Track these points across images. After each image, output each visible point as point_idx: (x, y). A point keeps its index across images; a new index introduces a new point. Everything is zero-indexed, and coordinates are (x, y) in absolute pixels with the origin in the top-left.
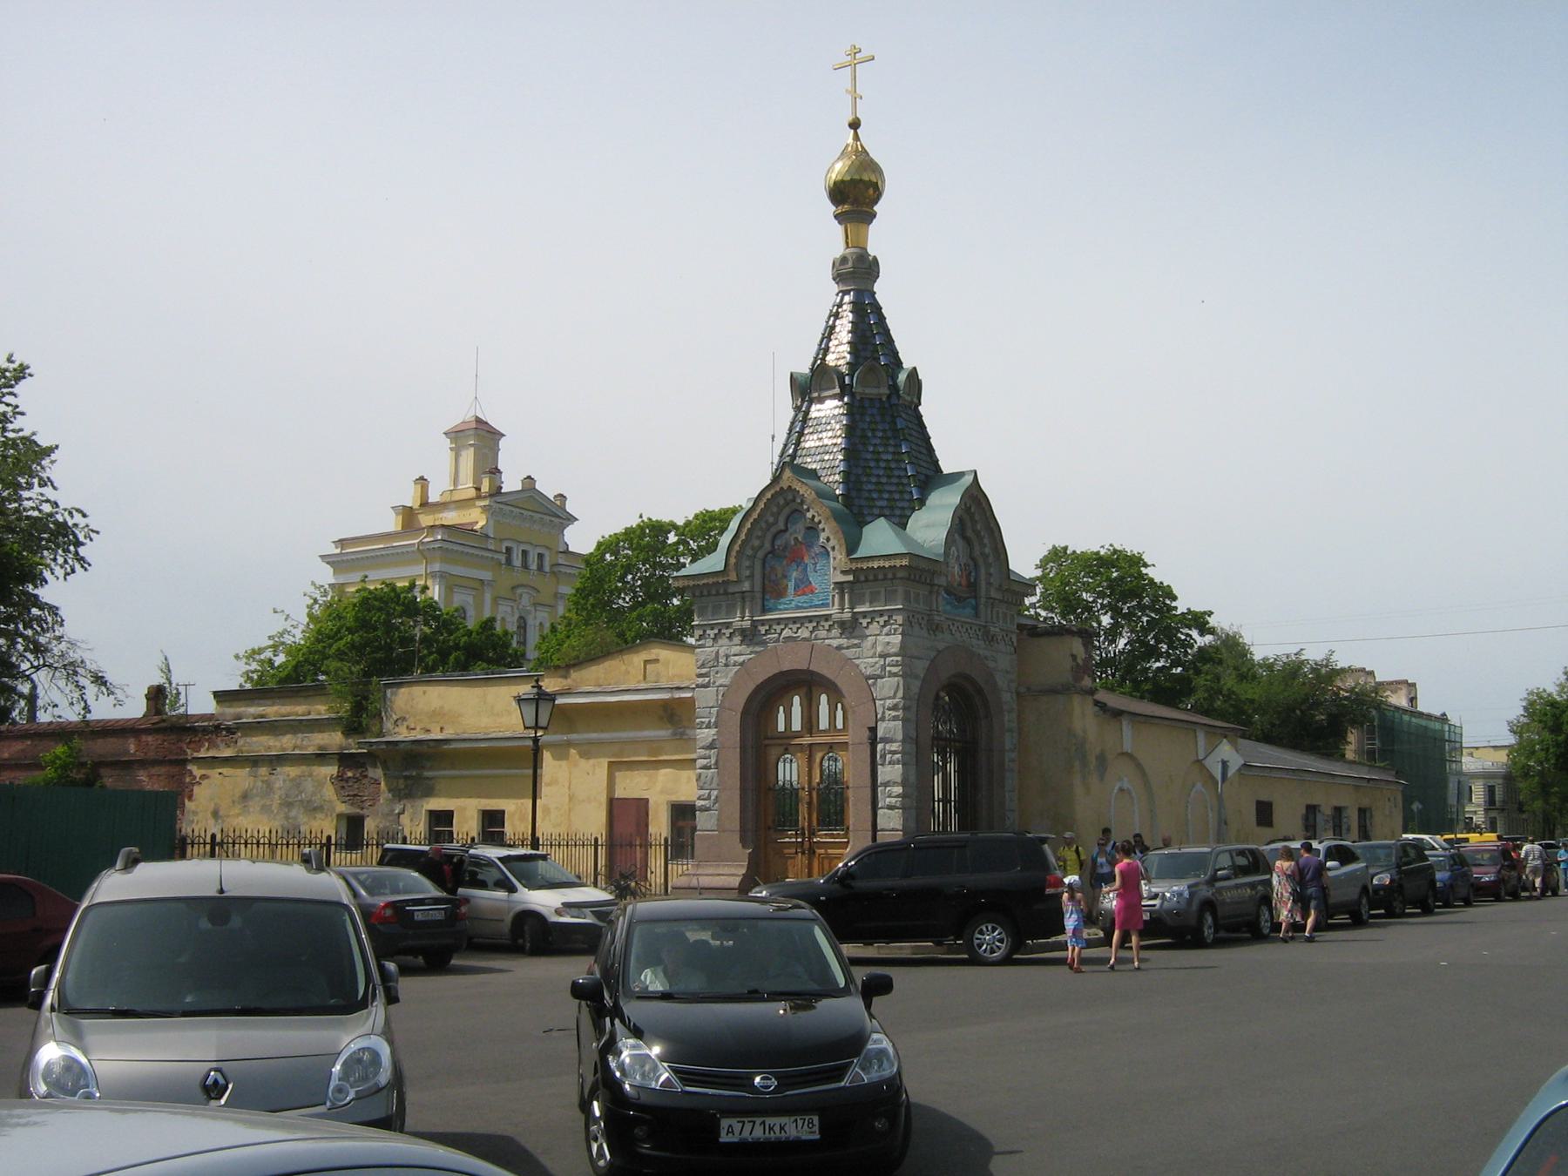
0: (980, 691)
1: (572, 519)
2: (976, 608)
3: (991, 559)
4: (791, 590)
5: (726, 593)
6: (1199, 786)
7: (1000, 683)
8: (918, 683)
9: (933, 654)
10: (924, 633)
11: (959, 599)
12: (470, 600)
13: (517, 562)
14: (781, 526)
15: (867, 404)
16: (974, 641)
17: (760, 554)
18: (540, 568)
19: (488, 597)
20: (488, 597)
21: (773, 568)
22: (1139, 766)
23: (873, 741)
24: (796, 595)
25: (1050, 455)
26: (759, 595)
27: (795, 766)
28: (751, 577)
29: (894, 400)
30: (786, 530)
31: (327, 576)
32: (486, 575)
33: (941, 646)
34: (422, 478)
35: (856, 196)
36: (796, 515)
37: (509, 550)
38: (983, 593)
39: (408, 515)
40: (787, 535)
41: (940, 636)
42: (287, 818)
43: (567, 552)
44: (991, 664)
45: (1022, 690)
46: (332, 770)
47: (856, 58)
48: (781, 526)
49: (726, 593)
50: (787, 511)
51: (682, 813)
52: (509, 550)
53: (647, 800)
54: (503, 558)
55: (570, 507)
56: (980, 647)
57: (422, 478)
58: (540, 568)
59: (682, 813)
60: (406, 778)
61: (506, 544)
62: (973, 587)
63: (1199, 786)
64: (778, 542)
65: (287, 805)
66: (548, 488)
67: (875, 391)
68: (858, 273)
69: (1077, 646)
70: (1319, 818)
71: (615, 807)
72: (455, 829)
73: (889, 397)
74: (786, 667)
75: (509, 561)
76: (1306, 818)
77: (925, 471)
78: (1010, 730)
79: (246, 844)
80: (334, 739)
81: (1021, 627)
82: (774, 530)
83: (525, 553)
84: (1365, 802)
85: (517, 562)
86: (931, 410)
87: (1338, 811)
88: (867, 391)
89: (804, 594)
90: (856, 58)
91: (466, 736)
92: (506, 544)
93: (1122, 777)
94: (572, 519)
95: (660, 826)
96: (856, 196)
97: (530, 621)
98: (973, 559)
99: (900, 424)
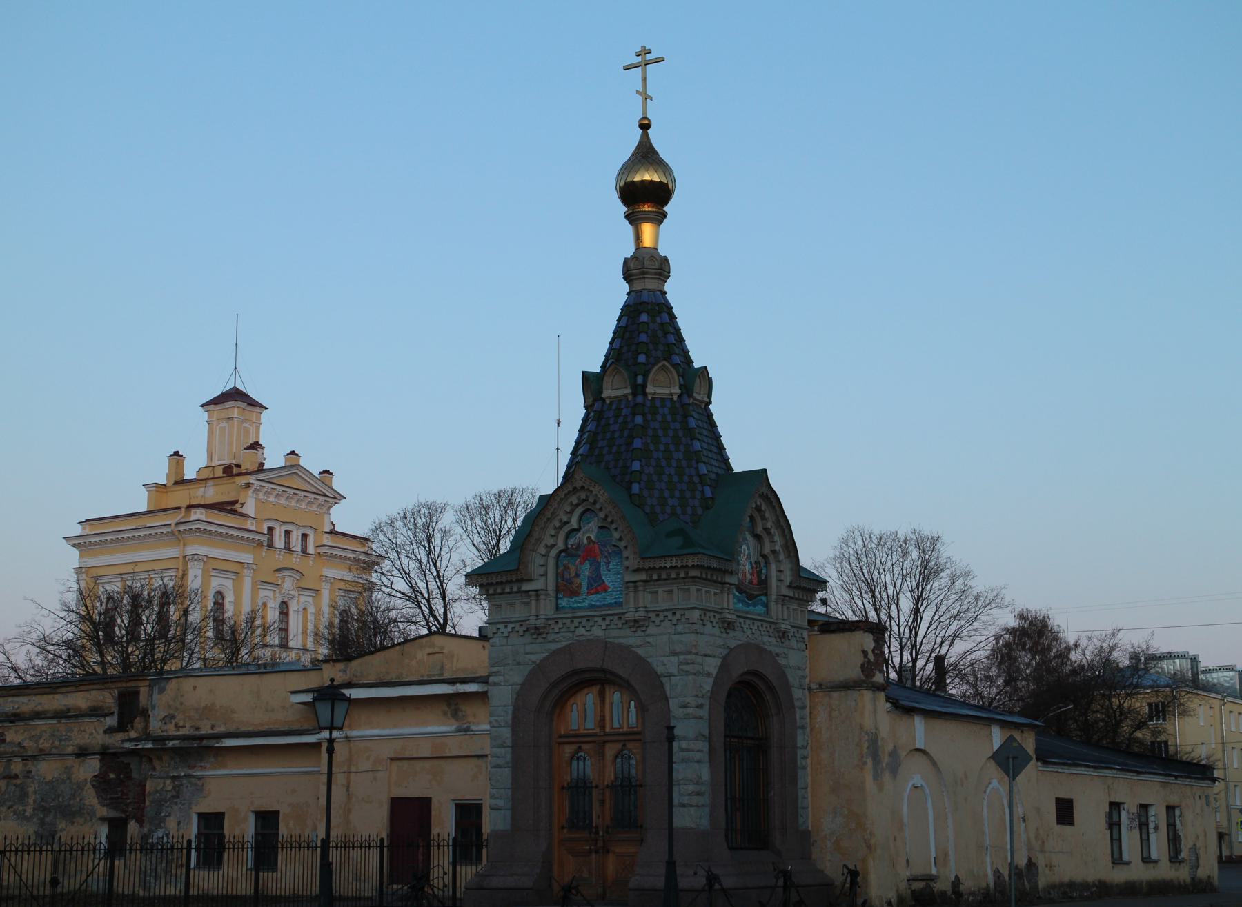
0: (771, 688)
1: (337, 497)
2: (766, 605)
3: (782, 557)
4: (584, 590)
5: (519, 591)
6: (995, 783)
7: (791, 679)
8: (711, 680)
9: (725, 652)
10: (716, 631)
11: (751, 597)
12: (229, 583)
13: (279, 542)
14: (574, 523)
15: (658, 404)
16: (766, 639)
17: (554, 553)
18: (304, 550)
19: (247, 582)
20: (247, 582)
21: (566, 568)
22: (934, 764)
23: (671, 739)
24: (589, 593)
25: (840, 447)
26: (552, 593)
27: (588, 763)
28: (545, 575)
29: (686, 400)
30: (578, 530)
31: (73, 557)
32: (247, 558)
33: (733, 644)
34: (177, 453)
35: (645, 197)
36: (588, 515)
37: (270, 529)
38: (774, 590)
39: (157, 489)
40: (579, 535)
41: (732, 634)
42: (42, 823)
43: (332, 532)
44: (782, 661)
45: (813, 686)
46: (92, 766)
47: (645, 59)
48: (574, 523)
49: (519, 591)
50: (579, 510)
51: (468, 813)
52: (270, 529)
53: (429, 799)
54: (264, 539)
55: (336, 484)
56: (769, 643)
57: (177, 453)
58: (304, 550)
59: (468, 813)
60: (174, 778)
61: (271, 524)
62: (763, 584)
63: (995, 783)
64: (571, 541)
65: (42, 808)
66: (312, 464)
67: (666, 391)
68: (646, 271)
69: (868, 641)
70: (1124, 814)
71: (399, 807)
72: (226, 832)
73: (680, 396)
74: (580, 665)
75: (270, 545)
76: (1110, 815)
77: (715, 470)
78: (803, 727)
79: (439, 846)
80: (94, 733)
81: (811, 623)
82: (567, 529)
83: (288, 533)
84: (1174, 799)
85: (279, 542)
86: (724, 410)
87: (1144, 807)
88: (659, 391)
89: (597, 592)
90: (645, 59)
91: (244, 729)
92: (271, 524)
93: (915, 775)
94: (337, 497)
95: (444, 824)
96: (645, 197)
97: (293, 607)
98: (764, 556)
99: (692, 423)
